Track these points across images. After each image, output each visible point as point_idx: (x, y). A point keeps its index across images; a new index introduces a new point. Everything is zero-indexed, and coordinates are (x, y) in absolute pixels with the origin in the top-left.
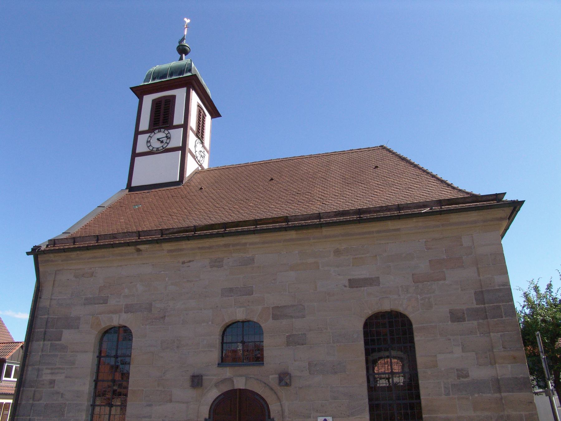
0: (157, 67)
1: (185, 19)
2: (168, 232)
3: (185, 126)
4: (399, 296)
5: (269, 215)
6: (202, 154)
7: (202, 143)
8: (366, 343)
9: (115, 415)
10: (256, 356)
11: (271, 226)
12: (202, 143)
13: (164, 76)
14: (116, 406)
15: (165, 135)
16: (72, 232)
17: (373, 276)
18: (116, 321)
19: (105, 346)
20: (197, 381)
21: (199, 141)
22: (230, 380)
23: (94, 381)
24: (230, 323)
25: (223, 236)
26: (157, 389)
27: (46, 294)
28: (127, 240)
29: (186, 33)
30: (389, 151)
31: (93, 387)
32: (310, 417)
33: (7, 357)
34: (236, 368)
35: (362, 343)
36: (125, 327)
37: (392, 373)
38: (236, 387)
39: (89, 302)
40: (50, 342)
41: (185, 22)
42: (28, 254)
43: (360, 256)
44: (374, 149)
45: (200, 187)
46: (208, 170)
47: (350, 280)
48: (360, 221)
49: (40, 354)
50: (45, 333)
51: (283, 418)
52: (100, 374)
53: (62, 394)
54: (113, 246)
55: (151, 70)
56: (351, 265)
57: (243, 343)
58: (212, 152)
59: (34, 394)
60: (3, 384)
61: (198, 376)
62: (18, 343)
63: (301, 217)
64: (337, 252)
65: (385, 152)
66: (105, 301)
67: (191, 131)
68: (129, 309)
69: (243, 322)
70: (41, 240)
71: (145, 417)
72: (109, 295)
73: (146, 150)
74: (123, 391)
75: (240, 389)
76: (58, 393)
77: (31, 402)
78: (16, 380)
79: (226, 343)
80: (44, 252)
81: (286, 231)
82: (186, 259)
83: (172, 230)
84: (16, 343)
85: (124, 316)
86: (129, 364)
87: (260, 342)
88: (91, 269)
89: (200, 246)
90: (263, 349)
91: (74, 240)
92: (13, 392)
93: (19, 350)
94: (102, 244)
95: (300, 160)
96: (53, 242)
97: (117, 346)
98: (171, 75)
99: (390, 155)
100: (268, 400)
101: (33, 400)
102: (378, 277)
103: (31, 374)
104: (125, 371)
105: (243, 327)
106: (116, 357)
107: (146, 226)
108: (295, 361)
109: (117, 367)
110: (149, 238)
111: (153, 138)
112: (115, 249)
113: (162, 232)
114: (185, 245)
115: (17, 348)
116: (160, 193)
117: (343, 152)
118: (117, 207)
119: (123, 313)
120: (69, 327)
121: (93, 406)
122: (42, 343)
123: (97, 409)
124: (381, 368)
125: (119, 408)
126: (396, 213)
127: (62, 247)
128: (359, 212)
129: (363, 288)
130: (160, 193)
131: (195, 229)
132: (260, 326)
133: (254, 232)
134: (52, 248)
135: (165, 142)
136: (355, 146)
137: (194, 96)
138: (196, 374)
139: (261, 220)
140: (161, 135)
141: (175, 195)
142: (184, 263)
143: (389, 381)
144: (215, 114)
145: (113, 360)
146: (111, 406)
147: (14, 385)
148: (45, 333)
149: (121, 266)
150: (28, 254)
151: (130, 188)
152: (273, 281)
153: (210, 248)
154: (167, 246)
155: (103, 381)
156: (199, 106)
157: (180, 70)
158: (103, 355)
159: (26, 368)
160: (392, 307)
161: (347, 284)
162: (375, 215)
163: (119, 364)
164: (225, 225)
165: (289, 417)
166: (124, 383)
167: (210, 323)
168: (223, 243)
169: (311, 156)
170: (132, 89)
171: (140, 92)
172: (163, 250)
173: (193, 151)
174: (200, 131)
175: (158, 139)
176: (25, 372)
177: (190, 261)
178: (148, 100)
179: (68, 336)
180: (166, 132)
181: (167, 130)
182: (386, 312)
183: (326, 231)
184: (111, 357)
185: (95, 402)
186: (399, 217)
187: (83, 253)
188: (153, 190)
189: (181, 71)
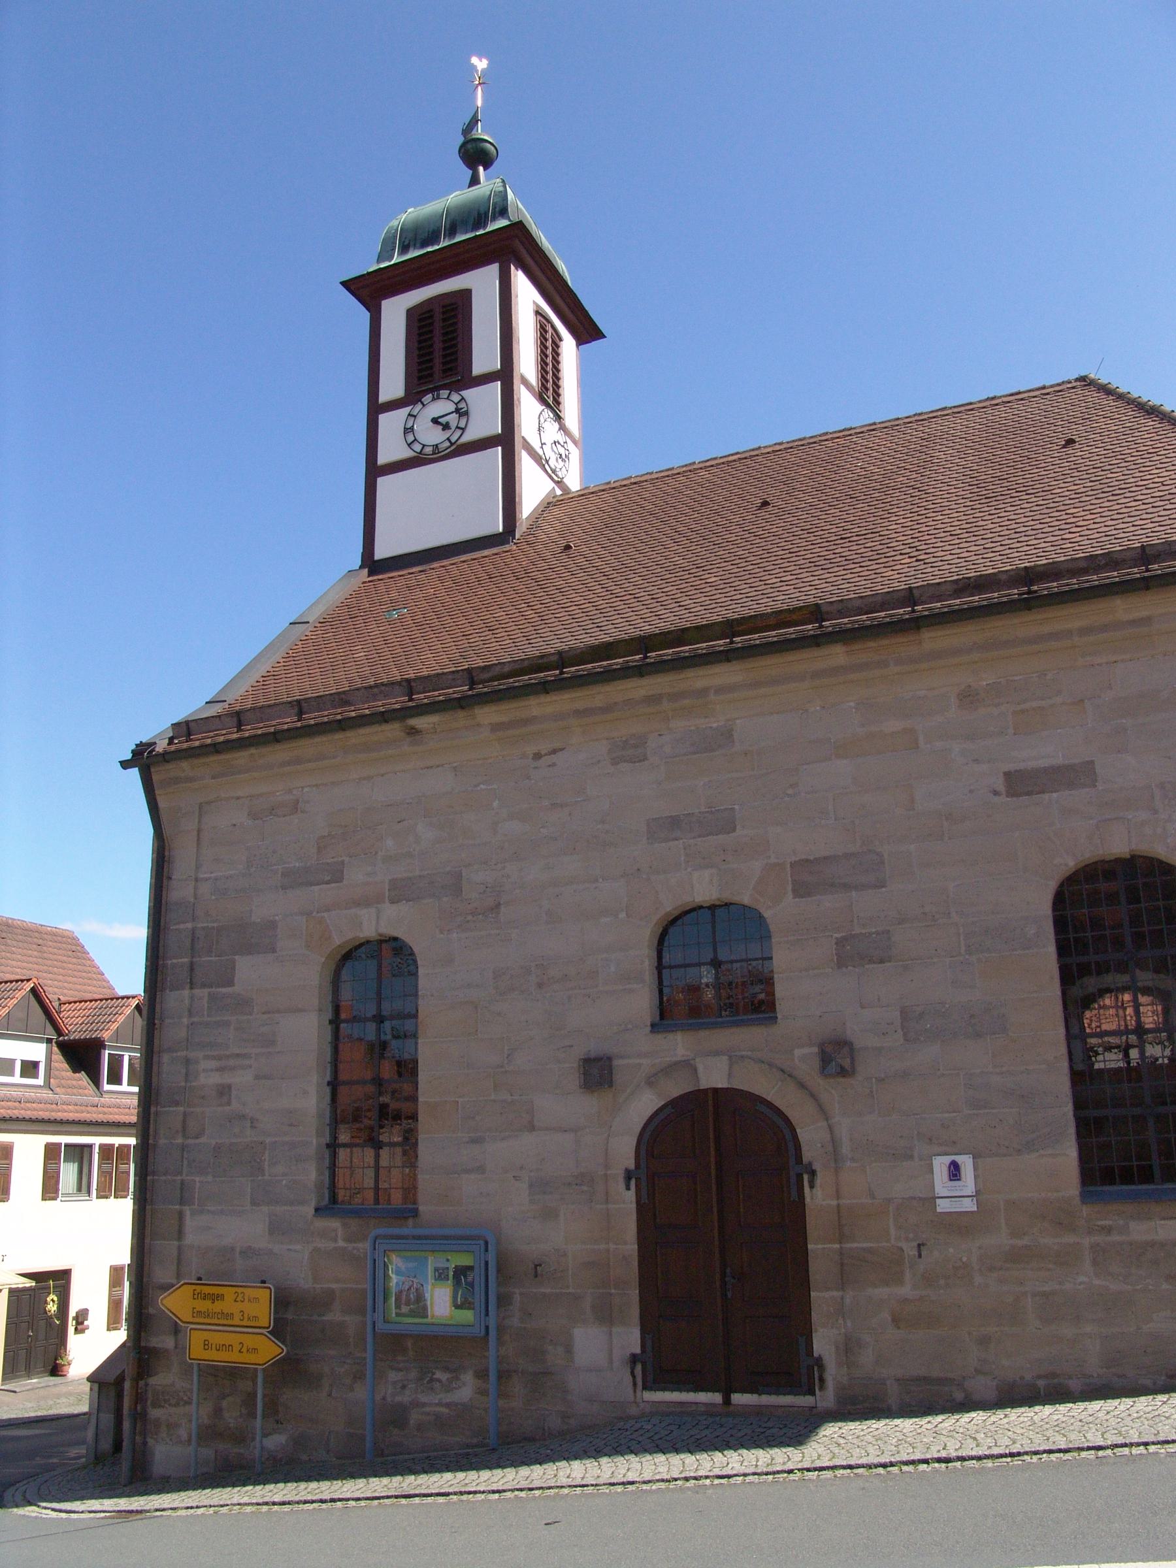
0: (410, 214)
1: (474, 60)
2: (486, 676)
3: (506, 374)
4: (1156, 812)
5: (765, 605)
6: (562, 451)
7: (558, 418)
8: (1062, 949)
9: (389, 1169)
10: (751, 1000)
11: (773, 635)
12: (558, 418)
13: (433, 238)
14: (392, 1145)
15: (452, 407)
16: (231, 697)
17: (1076, 761)
18: (370, 925)
19: (346, 995)
20: (597, 1073)
21: (548, 413)
22: (688, 1066)
23: (329, 1084)
24: (676, 913)
25: (641, 675)
26: (493, 1097)
27: (182, 868)
28: (380, 705)
29: (479, 103)
30: (1106, 390)
31: (328, 1098)
32: (911, 1157)
33: (106, 1035)
34: (703, 1034)
35: (1052, 949)
36: (395, 939)
37: (1140, 1030)
38: (704, 1084)
39: (295, 879)
40: (206, 991)
41: (474, 67)
42: (125, 765)
43: (1035, 704)
44: (1059, 389)
45: (563, 543)
46: (583, 495)
47: (1007, 775)
48: (1029, 603)
49: (185, 1021)
50: (192, 968)
51: (836, 1161)
52: (341, 1066)
53: (253, 1120)
54: (342, 725)
55: (395, 223)
56: (1011, 731)
57: (716, 963)
58: (589, 443)
59: (184, 1121)
60: (106, 1099)
61: (598, 1059)
62: (128, 998)
63: (858, 603)
64: (969, 698)
65: (1094, 396)
66: (337, 875)
67: (522, 388)
68: (401, 892)
69: (713, 908)
70: (154, 727)
71: (468, 1171)
72: (347, 859)
73: (407, 453)
74: (405, 1107)
75: (716, 1090)
76: (243, 1117)
77: (180, 1141)
78: (136, 1089)
79: (671, 967)
80: (165, 757)
81: (818, 645)
82: (544, 747)
83: (498, 669)
84: (123, 998)
85: (390, 911)
86: (415, 1036)
87: (763, 959)
88: (290, 791)
89: (579, 705)
90: (772, 978)
91: (238, 717)
92: (134, 1119)
93: (131, 1017)
94: (312, 722)
95: (829, 444)
96: (185, 729)
97: (379, 993)
98: (452, 231)
99: (1109, 401)
100: (793, 1115)
101: (185, 1136)
102: (1092, 762)
103: (169, 1071)
104: (406, 1056)
105: (713, 922)
106: (379, 1019)
107: (427, 663)
108: (863, 1007)
109: (384, 1045)
110: (438, 695)
111: (418, 420)
112: (349, 734)
113: (471, 676)
114: (537, 706)
115: (128, 1011)
116: (455, 571)
117: (969, 408)
118: (342, 620)
119: (387, 904)
120: (249, 949)
121: (333, 1146)
122: (186, 992)
123: (343, 1154)
124: (1106, 1017)
125: (399, 1150)
126: (1136, 572)
127: (209, 741)
128: (1028, 576)
129: (1046, 796)
130: (455, 571)
131: (563, 659)
132: (761, 917)
133: (727, 656)
134: (185, 746)
135: (453, 425)
136: (1002, 387)
137: (522, 284)
138: (593, 1055)
139: (743, 620)
140: (441, 407)
141: (495, 572)
142: (538, 756)
143: (1126, 1055)
144: (586, 330)
145: (371, 1027)
146: (378, 1146)
147: (135, 1101)
148: (192, 968)
149: (369, 778)
150: (125, 765)
151: (372, 564)
152: (790, 791)
153: (607, 709)
154: (488, 715)
155: (350, 1083)
156: (538, 313)
157: (476, 215)
158: (343, 1016)
159: (155, 1059)
160: (1134, 847)
161: (1000, 785)
162: (1074, 583)
163: (389, 1037)
164: (644, 643)
165: (853, 1159)
166: (407, 1088)
167: (622, 915)
168: (643, 692)
169: (872, 428)
170: (344, 284)
171: (369, 290)
172: (479, 725)
173: (536, 445)
174: (550, 385)
175: (435, 421)
176: (155, 1067)
177: (554, 752)
178: (395, 311)
179: (250, 972)
180: (455, 397)
181: (458, 390)
182: (1118, 860)
183: (933, 639)
184: (366, 1020)
185: (336, 1138)
186: (1146, 584)
187: (264, 750)
188: (435, 565)
189: (479, 215)
